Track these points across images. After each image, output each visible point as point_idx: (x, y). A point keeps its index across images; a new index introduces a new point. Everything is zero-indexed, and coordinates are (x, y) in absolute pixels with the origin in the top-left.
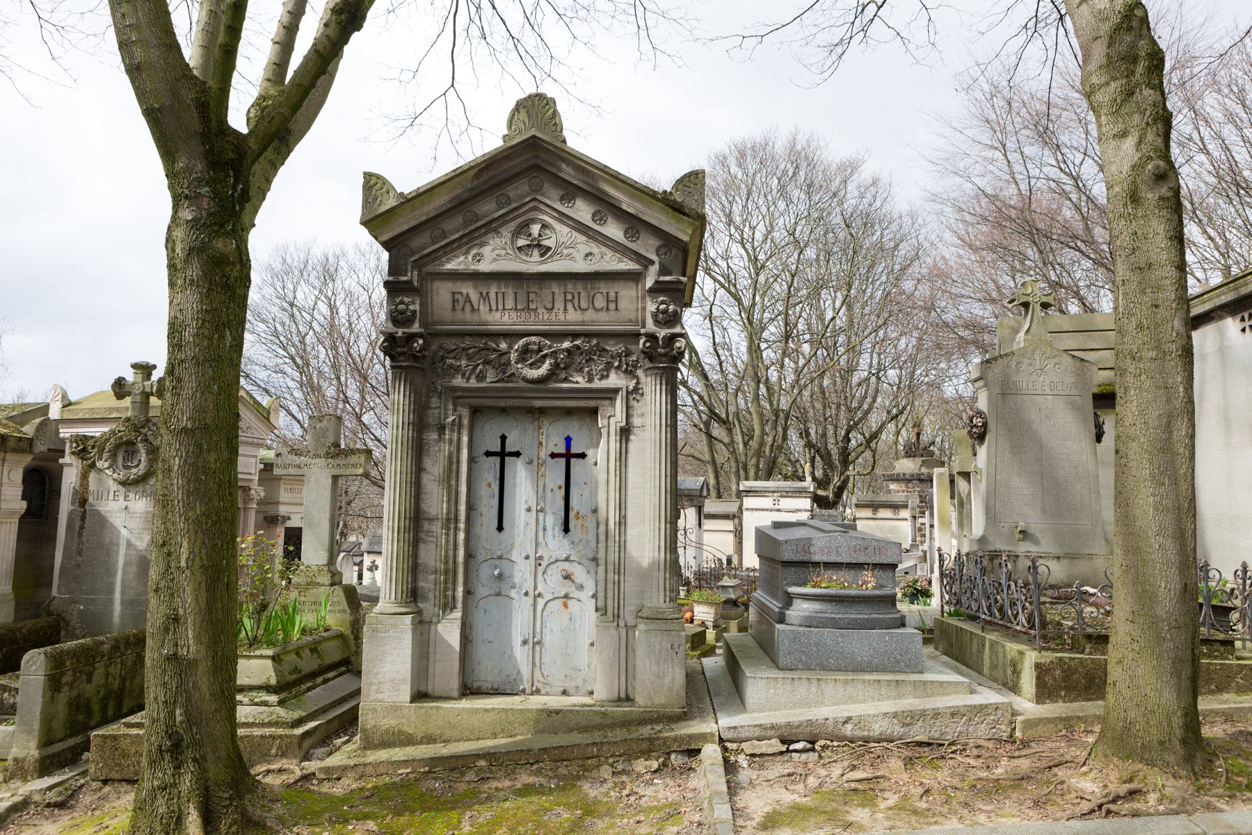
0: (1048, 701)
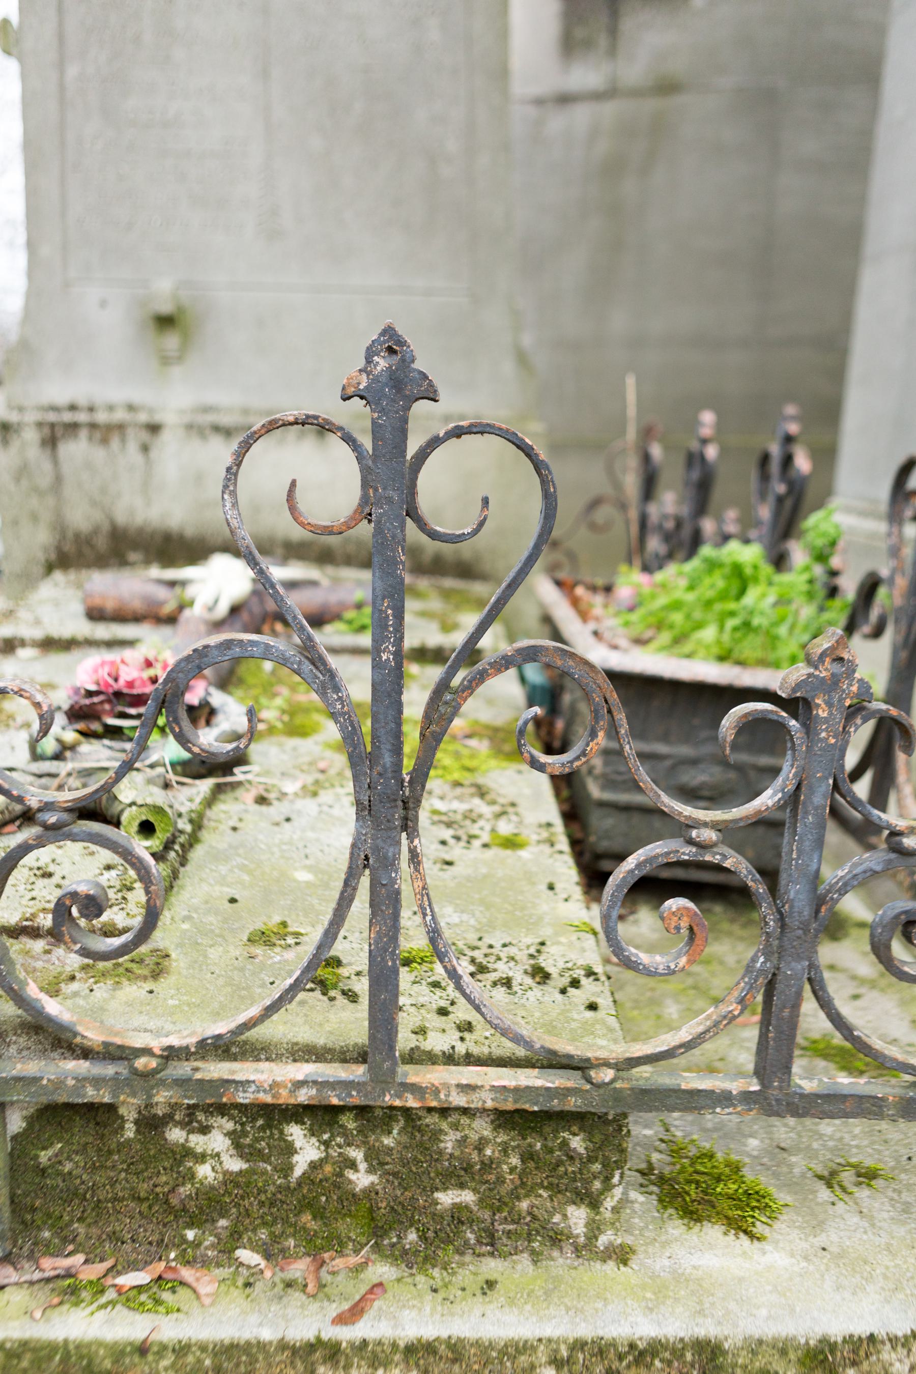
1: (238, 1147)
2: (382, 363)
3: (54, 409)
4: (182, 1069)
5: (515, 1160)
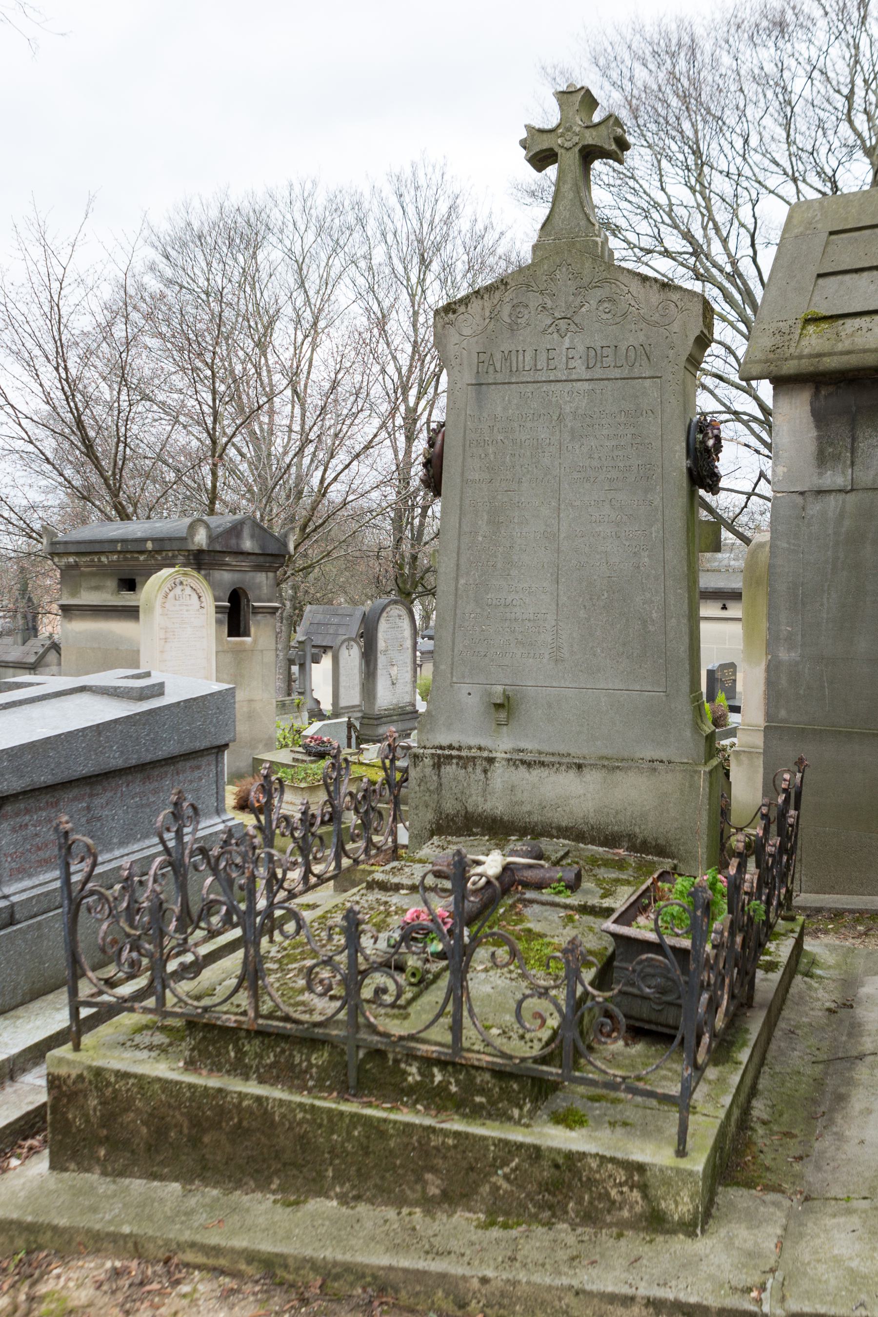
0: (72, 1166)
1: (420, 1073)
2: (456, 858)
3: (441, 748)
4: (404, 1043)
5: (497, 1089)
